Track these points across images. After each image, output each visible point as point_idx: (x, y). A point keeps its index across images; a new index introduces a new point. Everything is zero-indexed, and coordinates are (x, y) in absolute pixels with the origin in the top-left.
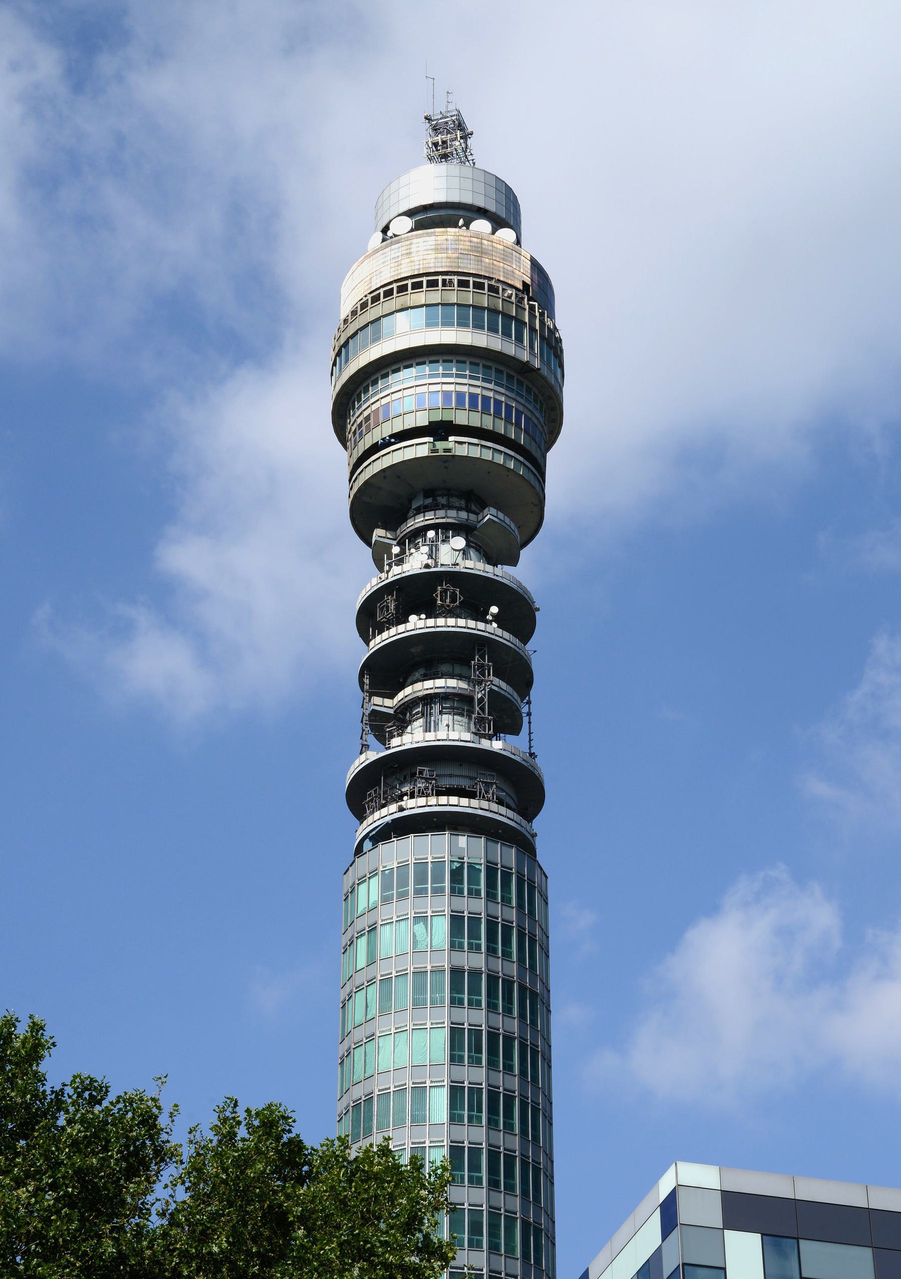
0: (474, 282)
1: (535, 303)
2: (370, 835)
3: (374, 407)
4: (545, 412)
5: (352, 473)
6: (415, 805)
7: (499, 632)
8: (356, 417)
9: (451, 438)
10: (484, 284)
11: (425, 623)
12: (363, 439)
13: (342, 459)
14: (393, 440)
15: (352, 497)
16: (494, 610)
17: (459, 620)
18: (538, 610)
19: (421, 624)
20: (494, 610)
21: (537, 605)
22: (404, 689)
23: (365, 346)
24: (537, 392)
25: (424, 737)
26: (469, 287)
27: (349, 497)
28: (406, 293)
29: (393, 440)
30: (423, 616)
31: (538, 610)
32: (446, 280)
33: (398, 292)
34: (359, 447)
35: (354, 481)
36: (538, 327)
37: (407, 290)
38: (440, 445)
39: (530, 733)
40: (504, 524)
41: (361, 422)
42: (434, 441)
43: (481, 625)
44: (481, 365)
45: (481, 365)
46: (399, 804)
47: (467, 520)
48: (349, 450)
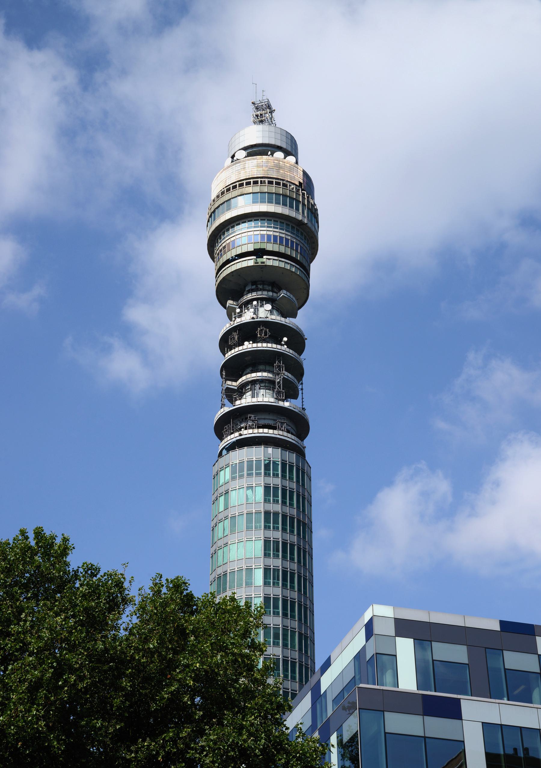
0: (275, 182)
1: (305, 192)
2: (226, 447)
3: (227, 242)
5: (217, 274)
7: (288, 350)
9: (265, 257)
11: (252, 346)
14: (236, 258)
15: (217, 285)
16: (285, 339)
18: (306, 339)
19: (250, 346)
20: (285, 339)
21: (306, 337)
26: (273, 184)
29: (236, 258)
30: (251, 342)
31: (306, 339)
32: (262, 181)
33: (239, 187)
35: (218, 278)
37: (243, 186)
38: (259, 260)
39: (302, 398)
40: (290, 298)
42: (256, 258)
43: (279, 347)
44: (279, 222)
45: (279, 222)
46: (240, 432)
47: (272, 296)
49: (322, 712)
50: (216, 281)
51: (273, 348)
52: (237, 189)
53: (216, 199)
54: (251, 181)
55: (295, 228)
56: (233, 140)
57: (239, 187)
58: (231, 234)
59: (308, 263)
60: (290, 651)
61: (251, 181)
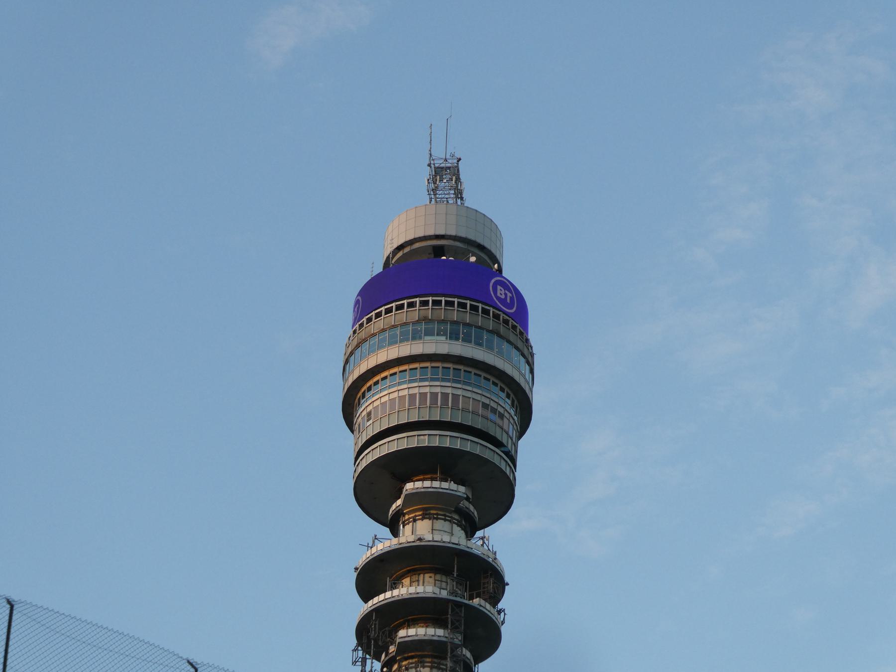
0: (458, 302)
1: (514, 309)
3: (376, 404)
4: (516, 407)
5: (356, 459)
6: (382, 356)
8: (361, 412)
10: (466, 304)
12: (365, 431)
13: (349, 442)
14: (463, 527)
15: (355, 478)
17: (460, 486)
18: (508, 584)
21: (507, 580)
22: (378, 595)
23: (371, 351)
24: (509, 392)
25: (433, 538)
27: (344, 389)
28: (402, 311)
31: (508, 584)
34: (356, 357)
35: (357, 465)
36: (450, 519)
41: (365, 391)
48: (356, 432)
49: (466, 390)
50: (355, 471)
51: (450, 490)
52: (405, 310)
53: (352, 336)
54: (429, 300)
55: (491, 381)
56: (505, 346)
57: (397, 310)
58: (381, 391)
59: (512, 440)
60: (461, 413)
61: (441, 300)
